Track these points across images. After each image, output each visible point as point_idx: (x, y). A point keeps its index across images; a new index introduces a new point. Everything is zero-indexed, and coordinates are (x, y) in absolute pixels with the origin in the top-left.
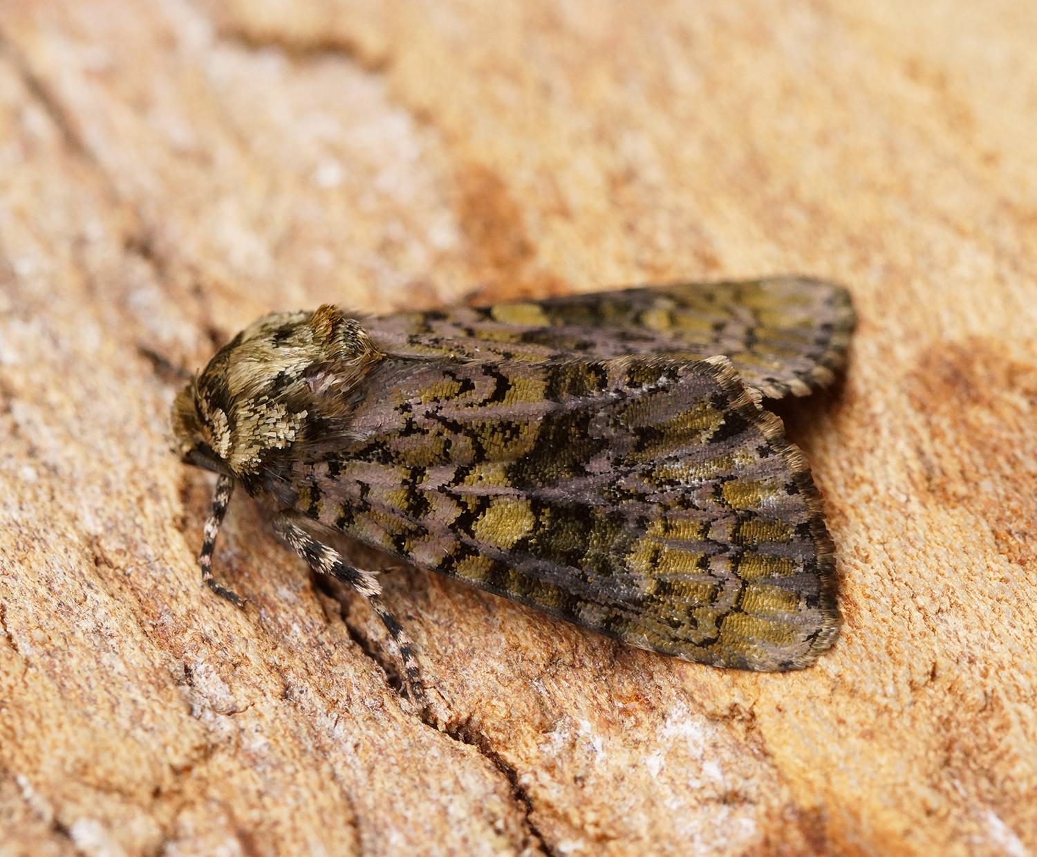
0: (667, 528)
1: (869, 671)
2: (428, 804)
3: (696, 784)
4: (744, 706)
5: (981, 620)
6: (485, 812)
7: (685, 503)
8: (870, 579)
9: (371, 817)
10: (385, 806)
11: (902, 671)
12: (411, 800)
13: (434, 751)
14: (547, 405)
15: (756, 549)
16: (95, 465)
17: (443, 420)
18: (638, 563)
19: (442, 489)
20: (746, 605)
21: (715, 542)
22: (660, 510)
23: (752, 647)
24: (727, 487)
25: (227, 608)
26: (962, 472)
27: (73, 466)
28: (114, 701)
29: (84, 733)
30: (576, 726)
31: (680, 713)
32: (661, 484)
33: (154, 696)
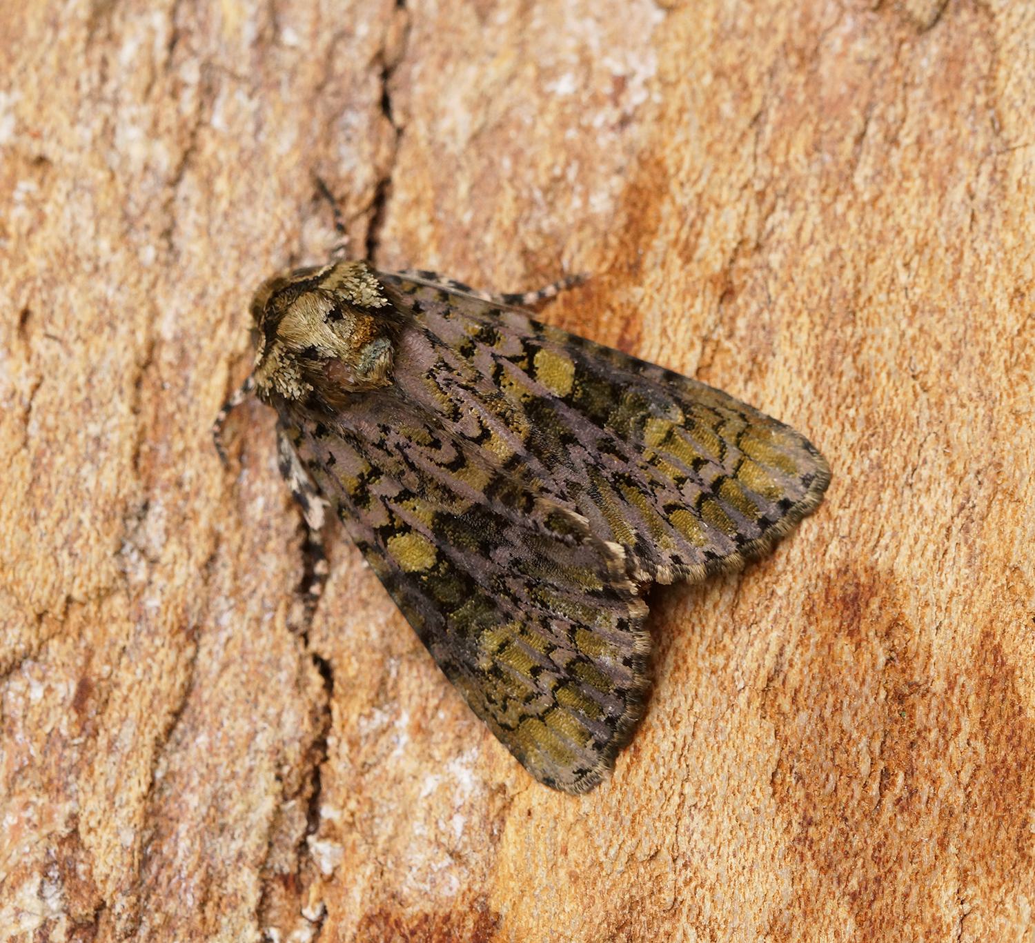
0: (523, 632)
1: (608, 827)
3: (442, 825)
4: (511, 791)
5: (717, 834)
6: (280, 756)
7: (545, 623)
8: (666, 746)
9: (198, 709)
10: (214, 705)
11: (631, 842)
12: (236, 711)
13: (283, 676)
14: (481, 498)
15: (579, 684)
16: (207, 270)
17: (406, 457)
18: (490, 641)
19: (383, 498)
20: (550, 719)
21: (552, 662)
22: (524, 617)
23: (536, 751)
24: (580, 633)
25: (215, 462)
26: (797, 691)
27: (189, 261)
28: (65, 514)
29: (22, 535)
32: (534, 600)
33: (98, 525)
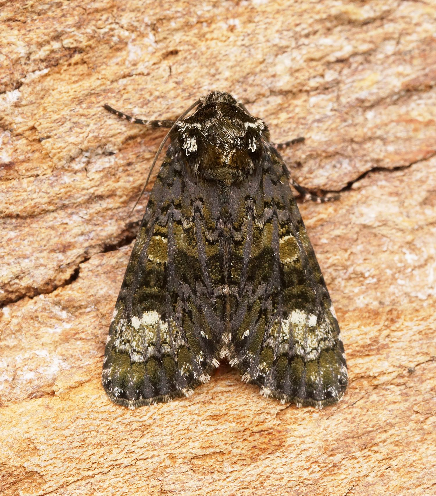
2: (31, 251)
10: (31, 232)
30: (67, 322)
31: (64, 366)
